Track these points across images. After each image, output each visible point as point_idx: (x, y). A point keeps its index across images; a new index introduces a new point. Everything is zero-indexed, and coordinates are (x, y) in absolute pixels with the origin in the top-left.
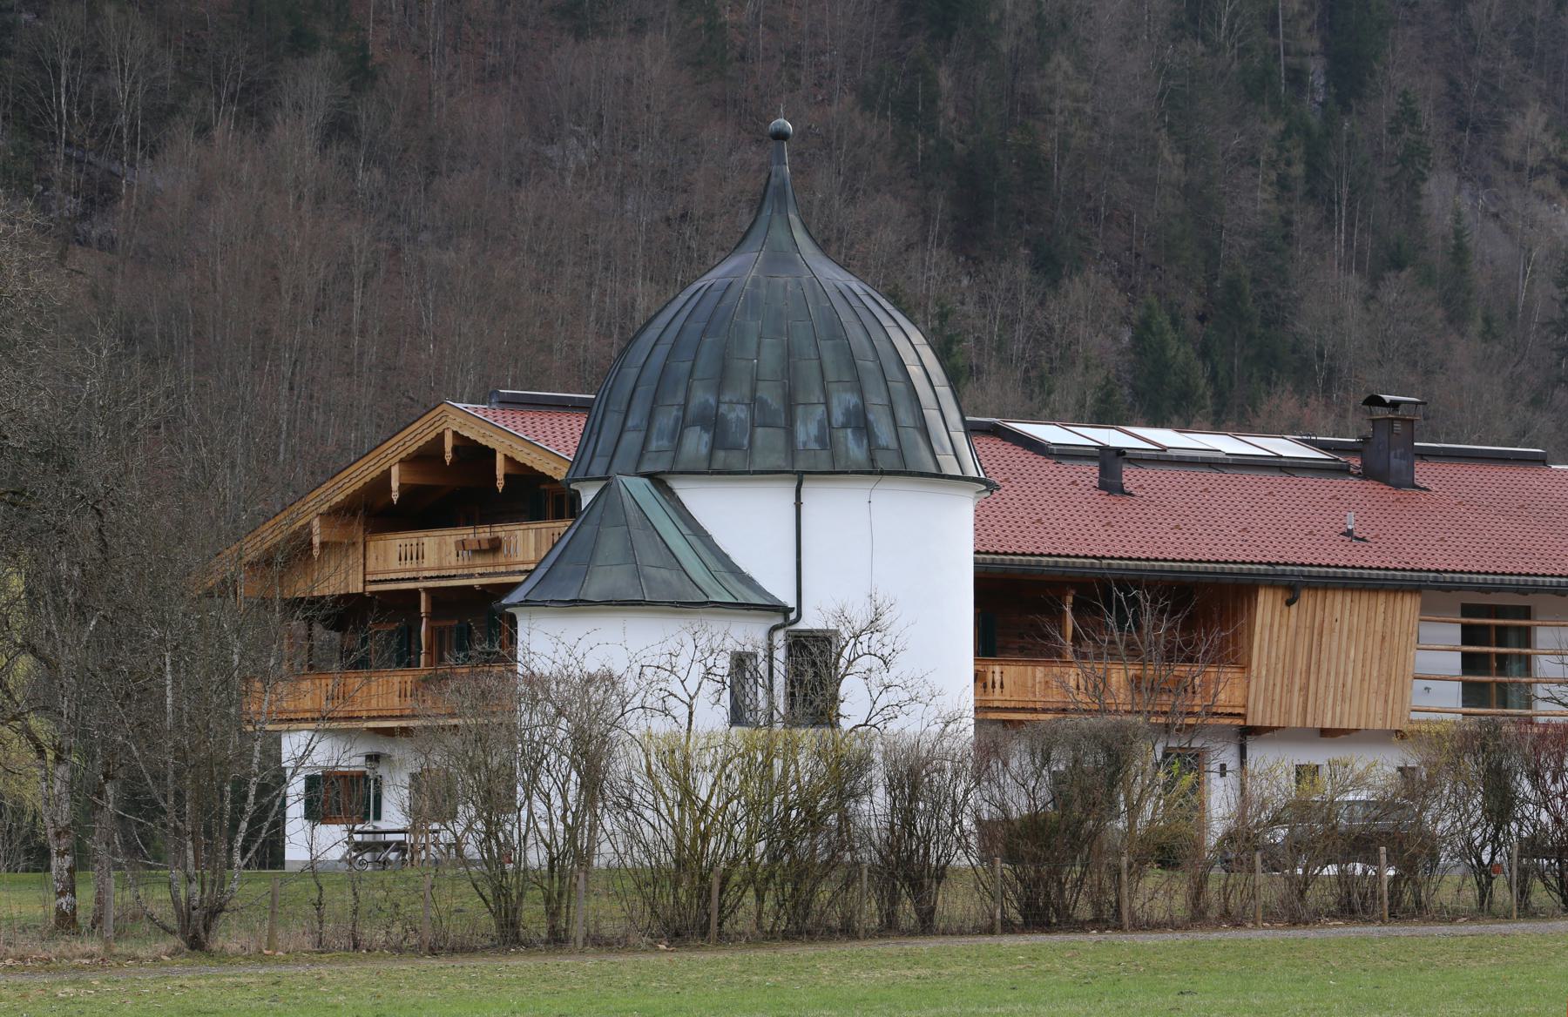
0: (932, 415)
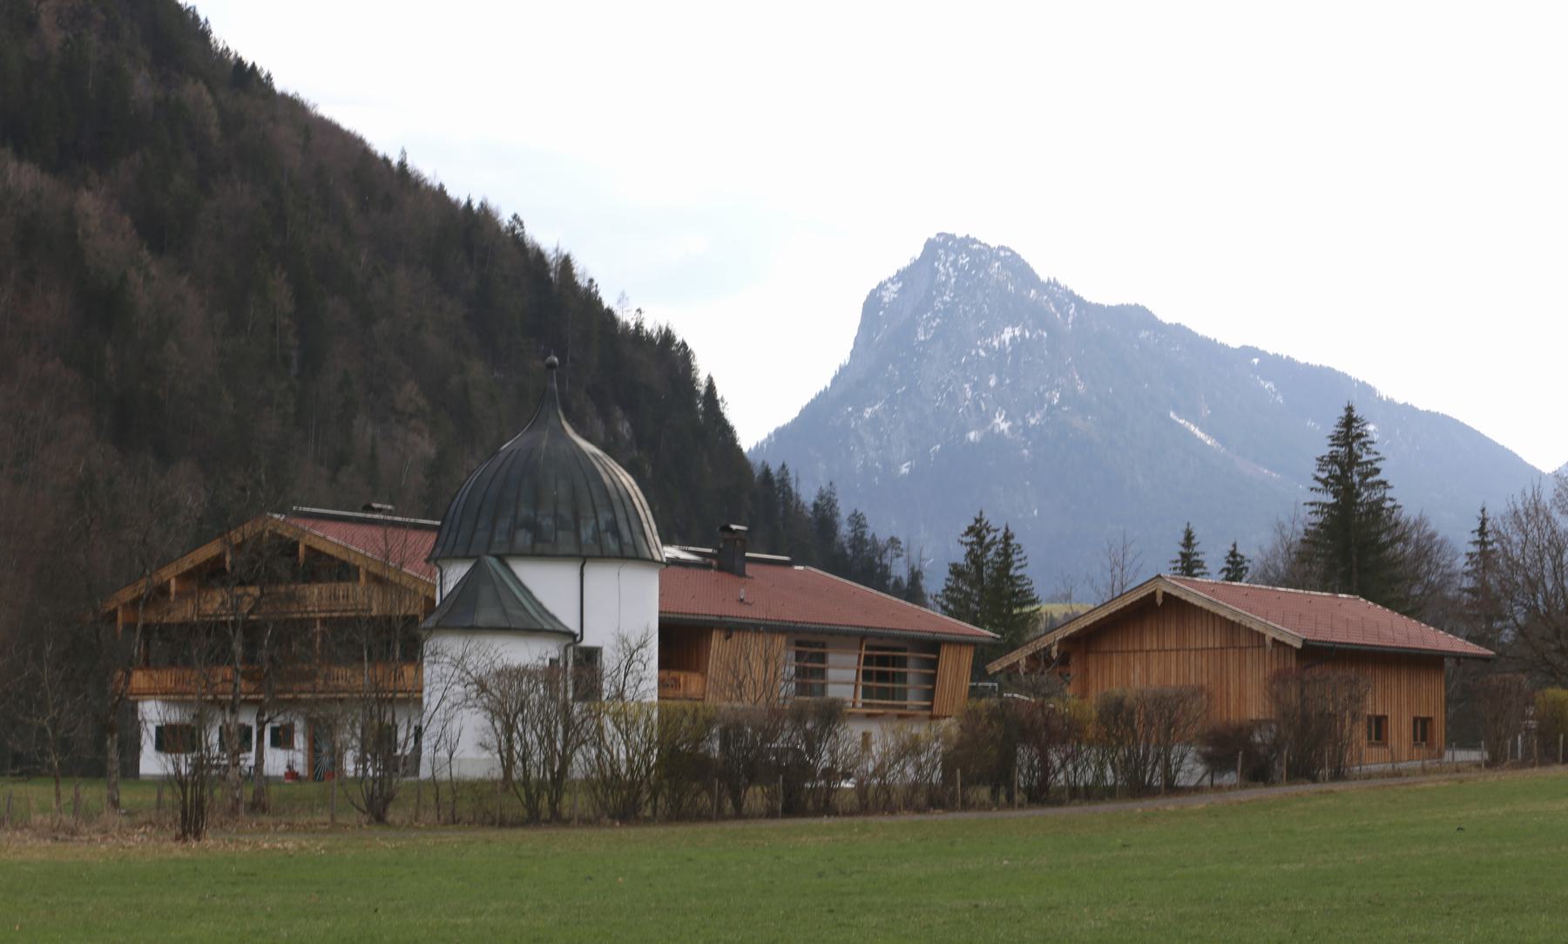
0: (646, 526)
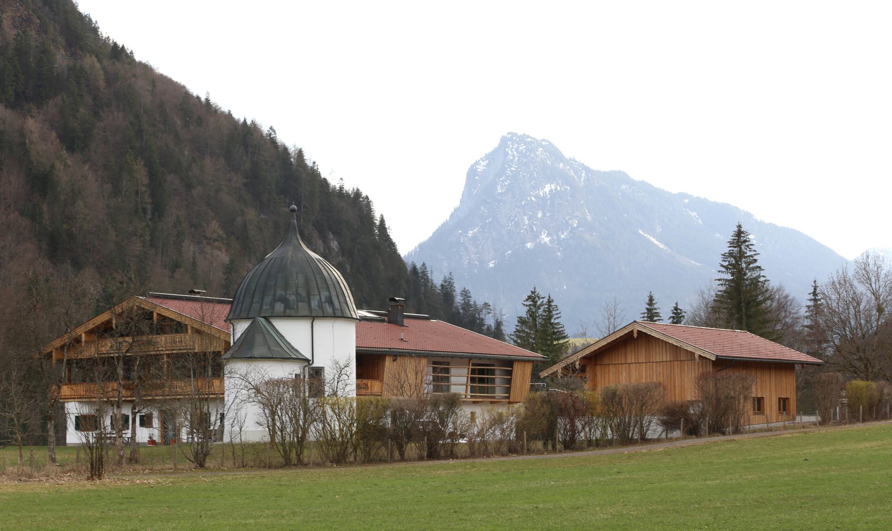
0: (348, 299)
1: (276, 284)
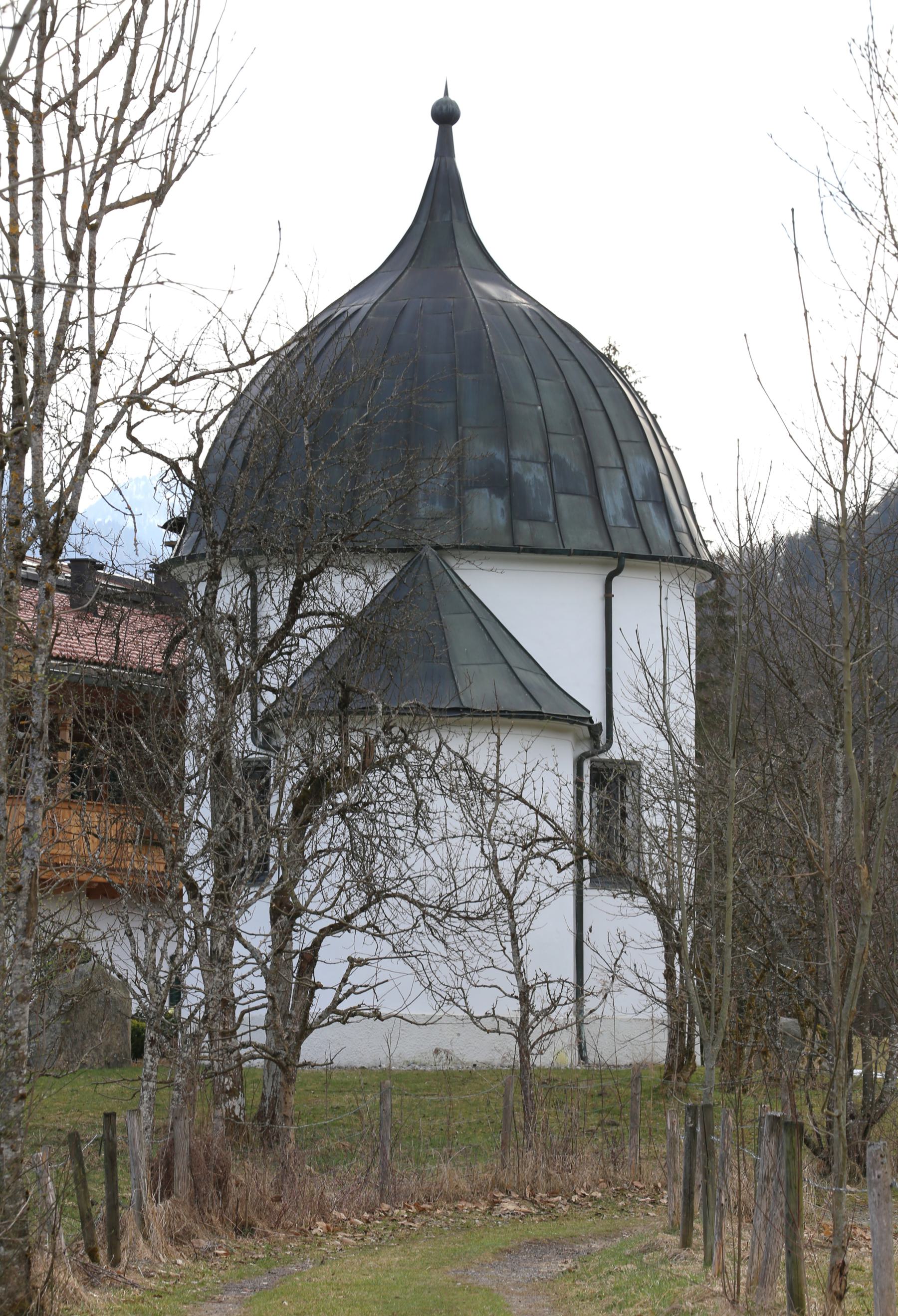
1: (457, 420)
